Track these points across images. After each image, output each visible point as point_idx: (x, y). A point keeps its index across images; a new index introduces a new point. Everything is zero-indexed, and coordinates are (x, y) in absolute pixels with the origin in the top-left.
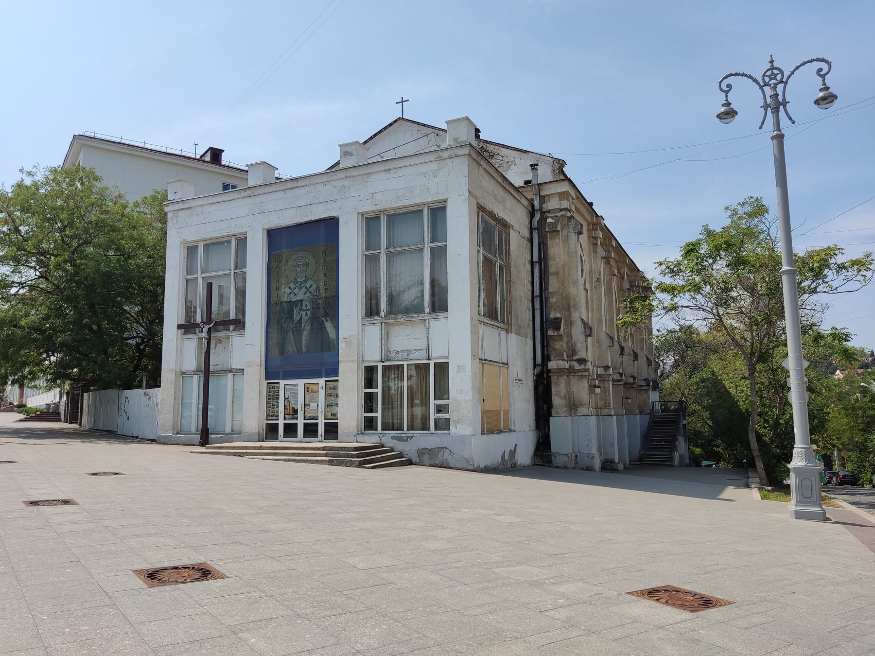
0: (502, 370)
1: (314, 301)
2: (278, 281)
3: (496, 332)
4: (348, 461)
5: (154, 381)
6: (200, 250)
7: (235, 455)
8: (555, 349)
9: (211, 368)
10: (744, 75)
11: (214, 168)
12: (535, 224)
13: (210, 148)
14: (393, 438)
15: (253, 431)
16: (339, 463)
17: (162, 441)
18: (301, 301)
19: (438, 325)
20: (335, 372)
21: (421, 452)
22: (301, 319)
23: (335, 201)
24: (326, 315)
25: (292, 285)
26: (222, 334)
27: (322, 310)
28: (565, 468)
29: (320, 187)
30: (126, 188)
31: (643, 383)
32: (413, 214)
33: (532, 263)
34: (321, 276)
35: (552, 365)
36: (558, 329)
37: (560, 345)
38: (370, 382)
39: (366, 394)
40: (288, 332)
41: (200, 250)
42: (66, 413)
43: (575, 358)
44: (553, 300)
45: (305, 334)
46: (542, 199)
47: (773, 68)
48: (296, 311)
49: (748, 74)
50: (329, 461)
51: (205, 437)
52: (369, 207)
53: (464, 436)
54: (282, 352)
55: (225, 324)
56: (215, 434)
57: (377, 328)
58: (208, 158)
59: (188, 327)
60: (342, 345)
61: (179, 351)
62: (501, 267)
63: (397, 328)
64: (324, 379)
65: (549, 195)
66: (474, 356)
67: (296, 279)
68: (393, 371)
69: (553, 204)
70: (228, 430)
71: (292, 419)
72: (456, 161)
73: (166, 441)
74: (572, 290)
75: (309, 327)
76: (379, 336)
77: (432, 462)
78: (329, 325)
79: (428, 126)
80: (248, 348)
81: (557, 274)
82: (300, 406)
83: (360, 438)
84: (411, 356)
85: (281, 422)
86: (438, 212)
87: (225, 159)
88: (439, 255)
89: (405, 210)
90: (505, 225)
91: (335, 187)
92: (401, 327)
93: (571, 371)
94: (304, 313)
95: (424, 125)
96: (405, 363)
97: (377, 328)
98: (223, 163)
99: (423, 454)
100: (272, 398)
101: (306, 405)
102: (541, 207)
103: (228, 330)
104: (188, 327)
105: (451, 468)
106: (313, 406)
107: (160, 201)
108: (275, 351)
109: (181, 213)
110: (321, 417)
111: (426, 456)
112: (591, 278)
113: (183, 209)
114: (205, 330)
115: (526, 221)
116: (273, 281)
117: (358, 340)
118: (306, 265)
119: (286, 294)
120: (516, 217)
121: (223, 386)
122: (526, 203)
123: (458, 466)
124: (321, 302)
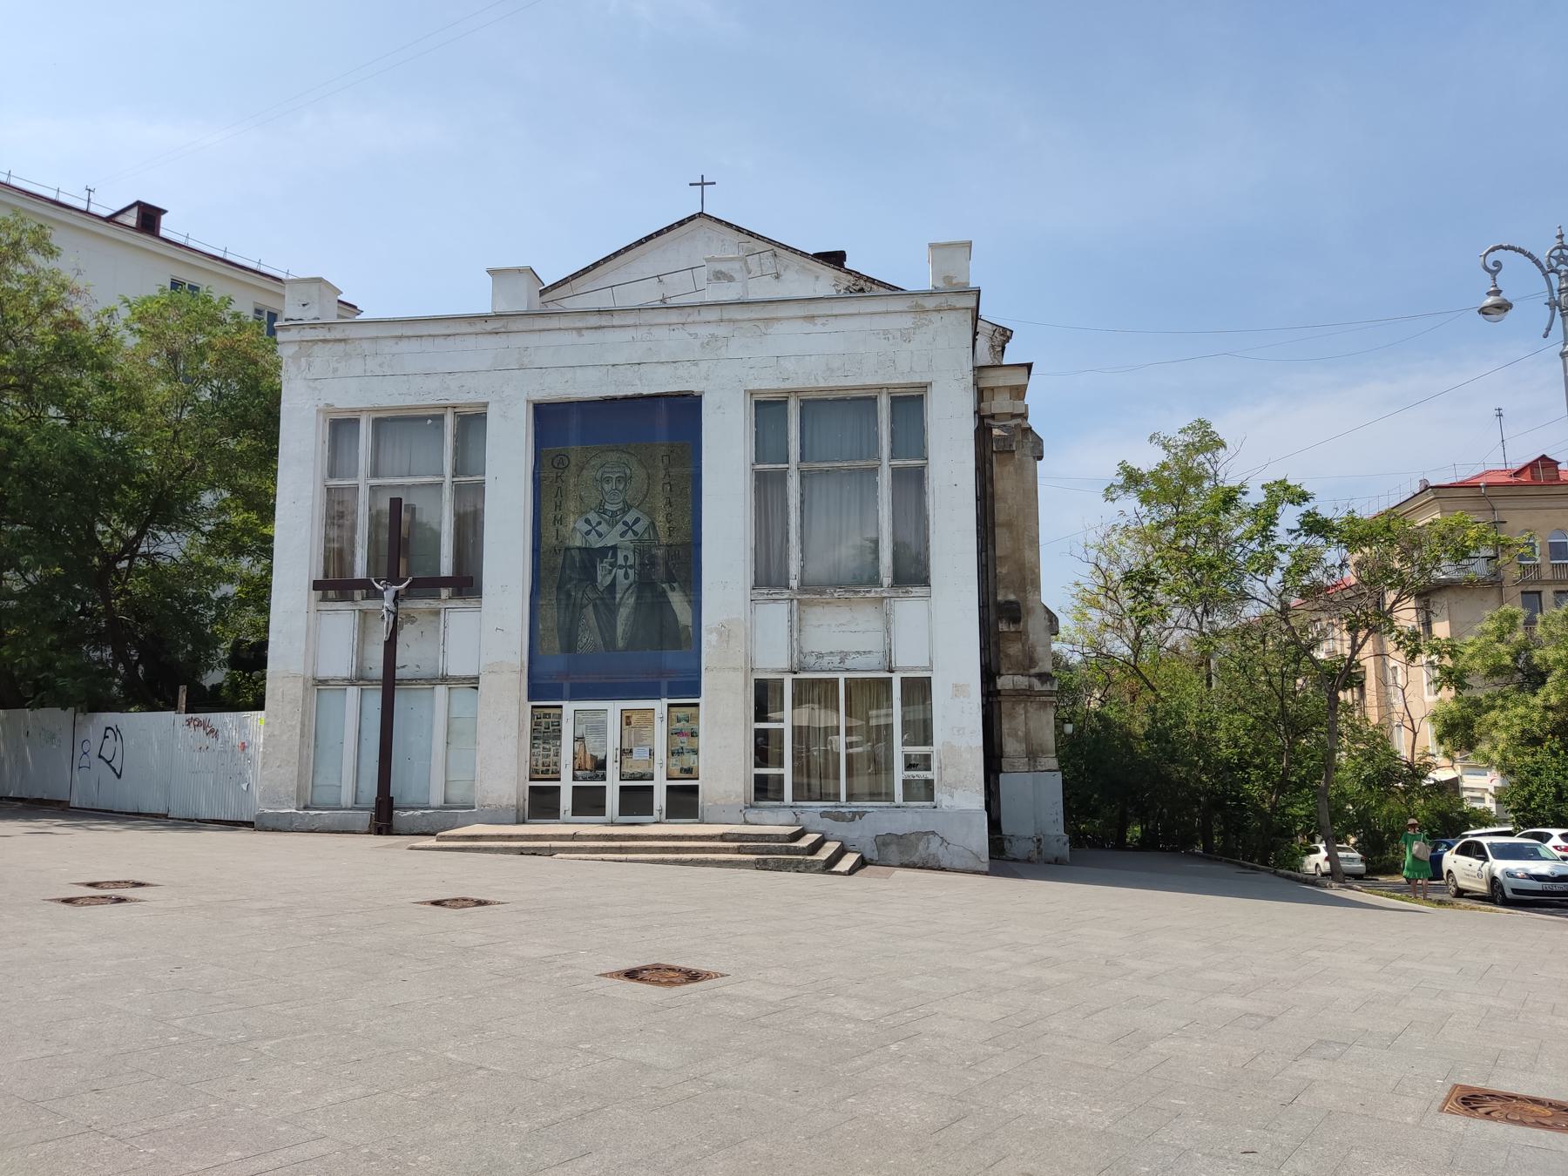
2: (558, 507)
4: (799, 862)
6: (365, 430)
7: (522, 852)
8: (1007, 656)
9: (399, 674)
10: (1520, 251)
11: (144, 240)
13: (138, 203)
14: (823, 815)
15: (505, 802)
16: (780, 866)
17: (270, 824)
18: (614, 548)
19: (908, 609)
20: (695, 690)
21: (883, 842)
22: (613, 584)
23: (695, 363)
24: (671, 579)
25: (593, 517)
26: (422, 604)
27: (661, 570)
28: (1029, 860)
29: (660, 333)
32: (861, 404)
34: (660, 503)
37: (1014, 649)
39: (758, 732)
40: (583, 607)
41: (365, 430)
43: (1033, 671)
44: (1003, 570)
45: (623, 613)
49: (1528, 250)
50: (758, 861)
51: (384, 819)
52: (769, 383)
53: (968, 812)
54: (569, 645)
55: (428, 585)
56: (405, 809)
58: (131, 219)
59: (334, 585)
60: (708, 640)
61: (313, 637)
63: (818, 610)
64: (666, 701)
65: (992, 389)
67: (601, 504)
68: (813, 691)
70: (436, 798)
71: (591, 779)
72: (950, 317)
73: (279, 824)
75: (632, 601)
76: (786, 624)
77: (905, 859)
78: (677, 600)
79: (760, 237)
80: (490, 633)
81: (1009, 525)
83: (752, 815)
84: (848, 664)
87: (167, 227)
88: (912, 482)
89: (841, 395)
91: (696, 336)
92: (827, 609)
94: (621, 572)
95: (751, 234)
96: (842, 677)
98: (163, 233)
99: (885, 844)
101: (625, 752)
103: (437, 596)
104: (334, 585)
105: (943, 869)
106: (640, 754)
107: (269, 321)
108: (553, 645)
109: (317, 349)
111: (894, 847)
113: (325, 341)
117: (740, 627)
118: (625, 479)
119: (576, 531)
123: (957, 864)
124: (660, 552)
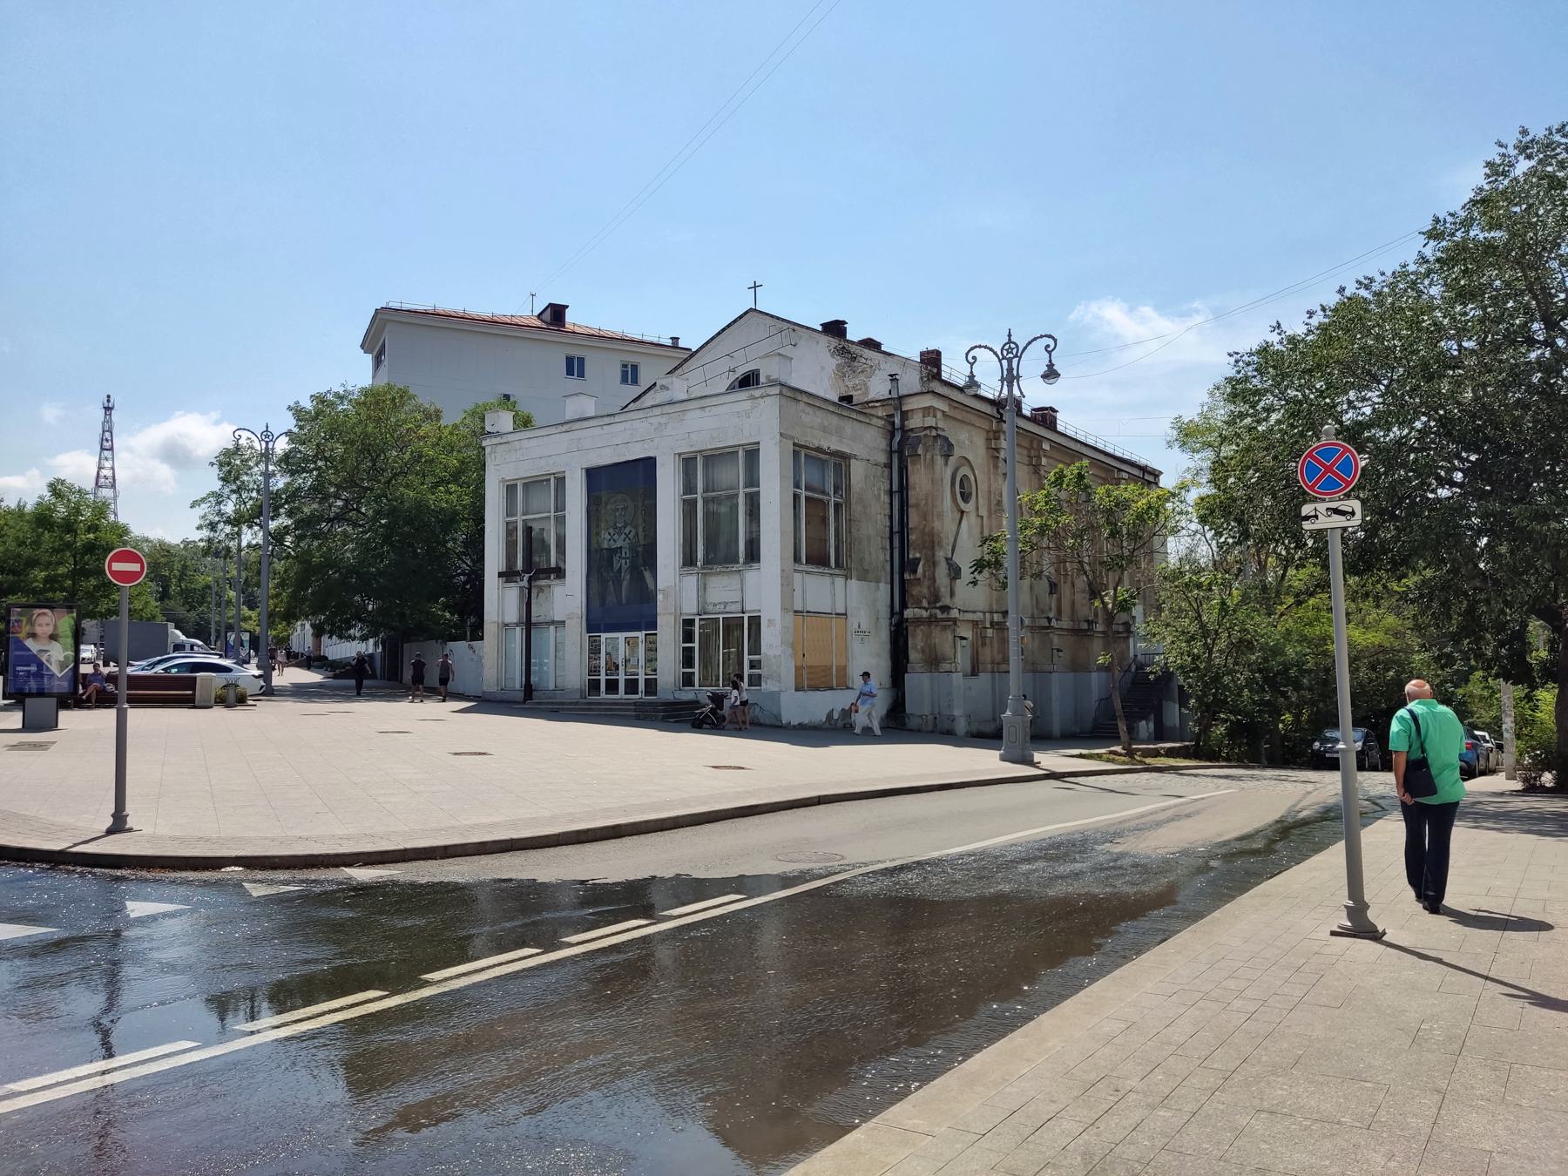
0: (841, 620)
1: (633, 548)
3: (827, 580)
5: (477, 633)
6: (520, 489)
9: (533, 620)
12: (895, 447)
26: (543, 583)
28: (919, 731)
29: (637, 424)
30: (446, 393)
31: (1121, 629)
33: (891, 493)
35: (908, 613)
36: (915, 572)
38: (688, 637)
41: (520, 489)
42: (383, 667)
44: (912, 537)
46: (905, 415)
47: (1010, 342)
48: (616, 559)
52: (685, 448)
54: (603, 604)
57: (694, 578)
60: (660, 597)
61: (501, 600)
62: (837, 506)
66: (784, 609)
69: (915, 422)
70: (552, 686)
72: (768, 400)
74: (937, 525)
78: (647, 575)
80: (568, 598)
81: (917, 506)
82: (620, 661)
85: (603, 678)
86: (752, 454)
90: (842, 460)
93: (932, 620)
97: (694, 578)
100: (595, 650)
101: (627, 661)
102: (903, 426)
104: (508, 575)
108: (596, 603)
110: (641, 672)
112: (989, 500)
114: (526, 577)
115: (883, 444)
116: (593, 525)
117: (676, 588)
118: (625, 509)
119: (606, 541)
120: (864, 445)
121: (546, 639)
122: (881, 423)
